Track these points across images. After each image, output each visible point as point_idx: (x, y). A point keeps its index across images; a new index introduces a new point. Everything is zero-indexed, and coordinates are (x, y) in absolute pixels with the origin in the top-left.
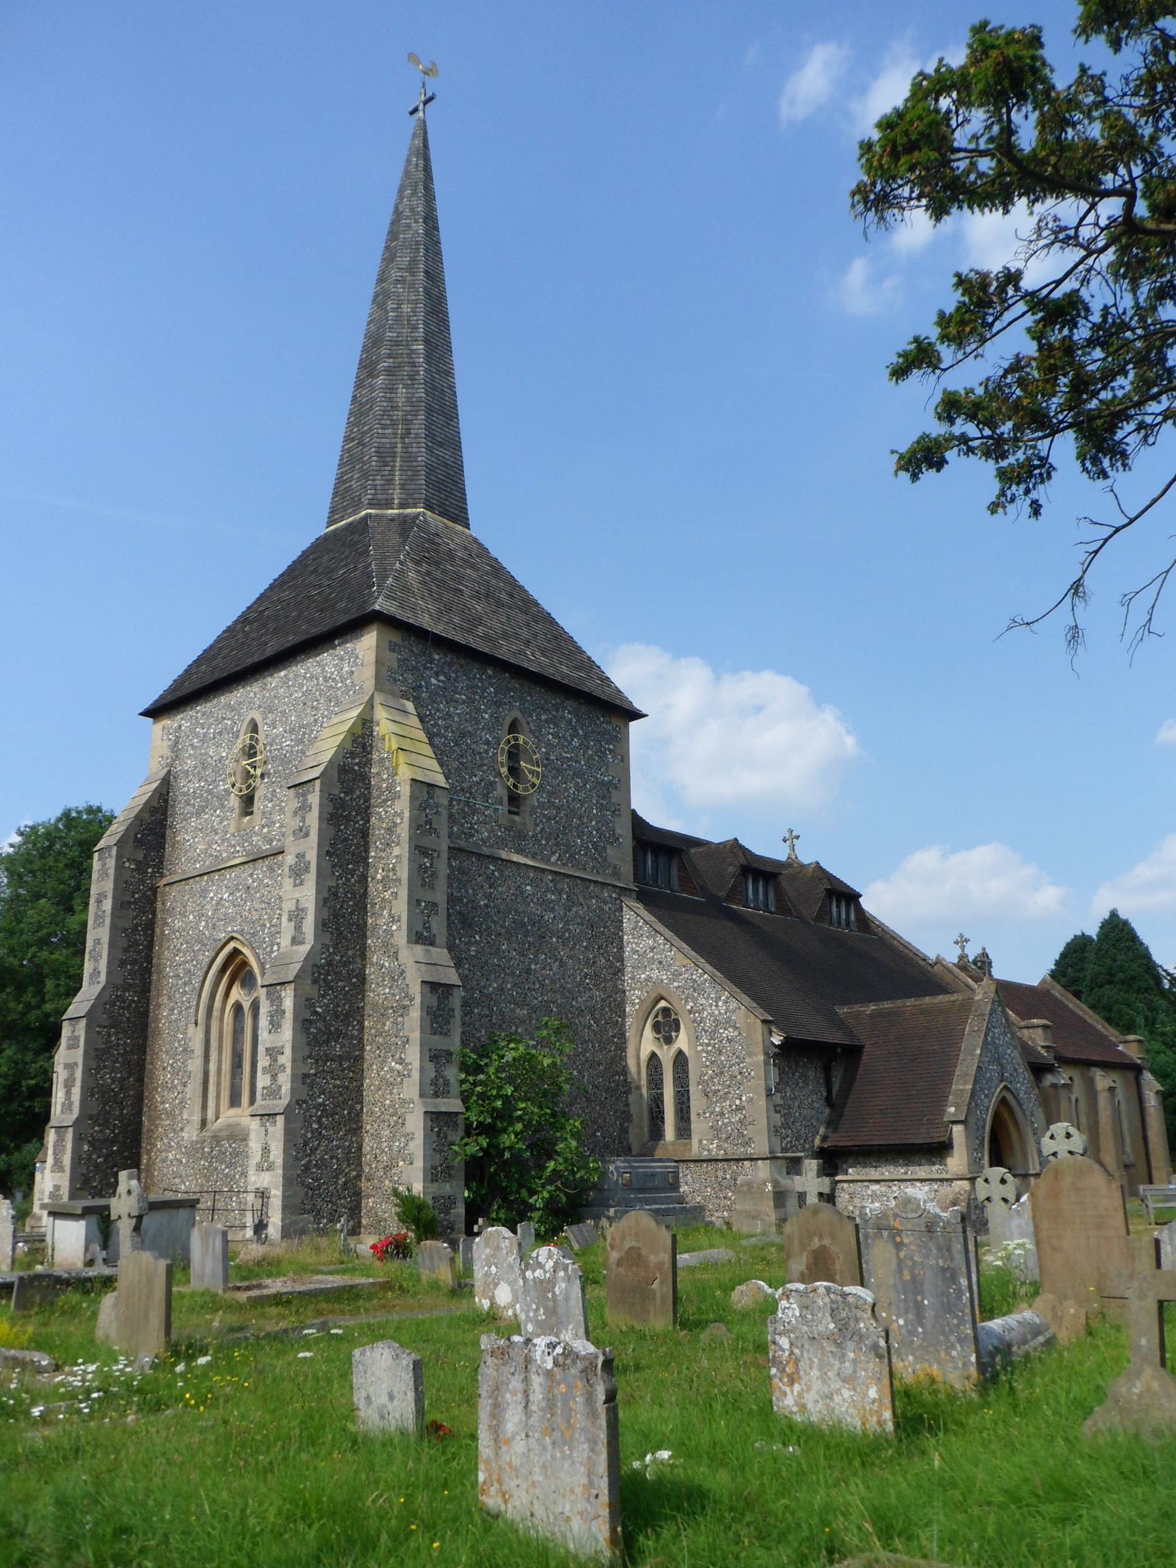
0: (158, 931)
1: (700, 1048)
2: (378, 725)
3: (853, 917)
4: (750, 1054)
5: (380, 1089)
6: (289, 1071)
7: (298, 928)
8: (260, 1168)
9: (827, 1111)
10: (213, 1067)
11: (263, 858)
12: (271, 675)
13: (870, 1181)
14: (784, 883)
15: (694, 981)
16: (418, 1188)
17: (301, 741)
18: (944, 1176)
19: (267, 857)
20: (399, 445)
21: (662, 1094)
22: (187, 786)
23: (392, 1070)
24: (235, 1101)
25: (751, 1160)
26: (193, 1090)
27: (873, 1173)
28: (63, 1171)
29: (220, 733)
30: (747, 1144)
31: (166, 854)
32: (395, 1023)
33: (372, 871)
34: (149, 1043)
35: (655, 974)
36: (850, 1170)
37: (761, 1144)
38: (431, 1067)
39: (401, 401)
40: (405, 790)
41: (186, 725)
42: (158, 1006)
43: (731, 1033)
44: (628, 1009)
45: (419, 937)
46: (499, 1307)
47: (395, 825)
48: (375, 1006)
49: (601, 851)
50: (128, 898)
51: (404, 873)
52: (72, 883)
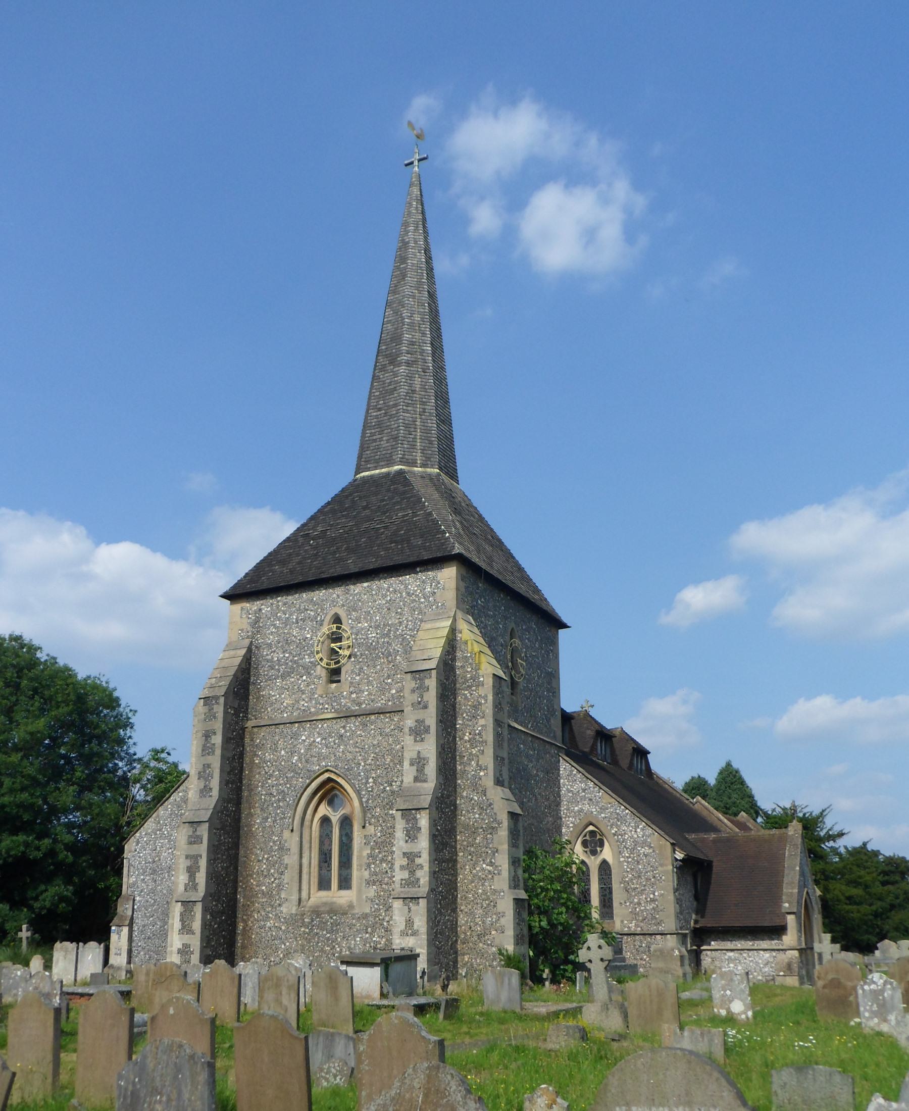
0: (247, 760)
1: (622, 859)
2: (461, 632)
3: (644, 768)
4: (661, 865)
5: (473, 882)
6: (426, 868)
7: (421, 770)
8: (404, 934)
9: (695, 903)
10: (305, 861)
11: (356, 716)
12: (354, 584)
13: (727, 950)
14: (616, 745)
15: (618, 814)
16: (510, 948)
17: (388, 635)
18: (781, 947)
19: (359, 716)
20: (419, 420)
21: (589, 889)
22: (272, 655)
23: (483, 870)
24: (324, 884)
25: (662, 934)
26: (289, 877)
27: (729, 945)
28: (193, 933)
29: (303, 620)
30: (659, 924)
31: (251, 703)
32: (485, 838)
33: (459, 734)
34: (243, 841)
35: (586, 808)
36: (713, 943)
37: (670, 923)
38: (512, 868)
39: (418, 388)
40: (489, 682)
41: (266, 609)
42: (251, 815)
43: (647, 850)
44: (564, 830)
45: (499, 782)
46: (733, 1014)
47: (480, 704)
48: (467, 827)
49: (548, 721)
50: (230, 735)
51: (489, 737)
52: (14, 699)
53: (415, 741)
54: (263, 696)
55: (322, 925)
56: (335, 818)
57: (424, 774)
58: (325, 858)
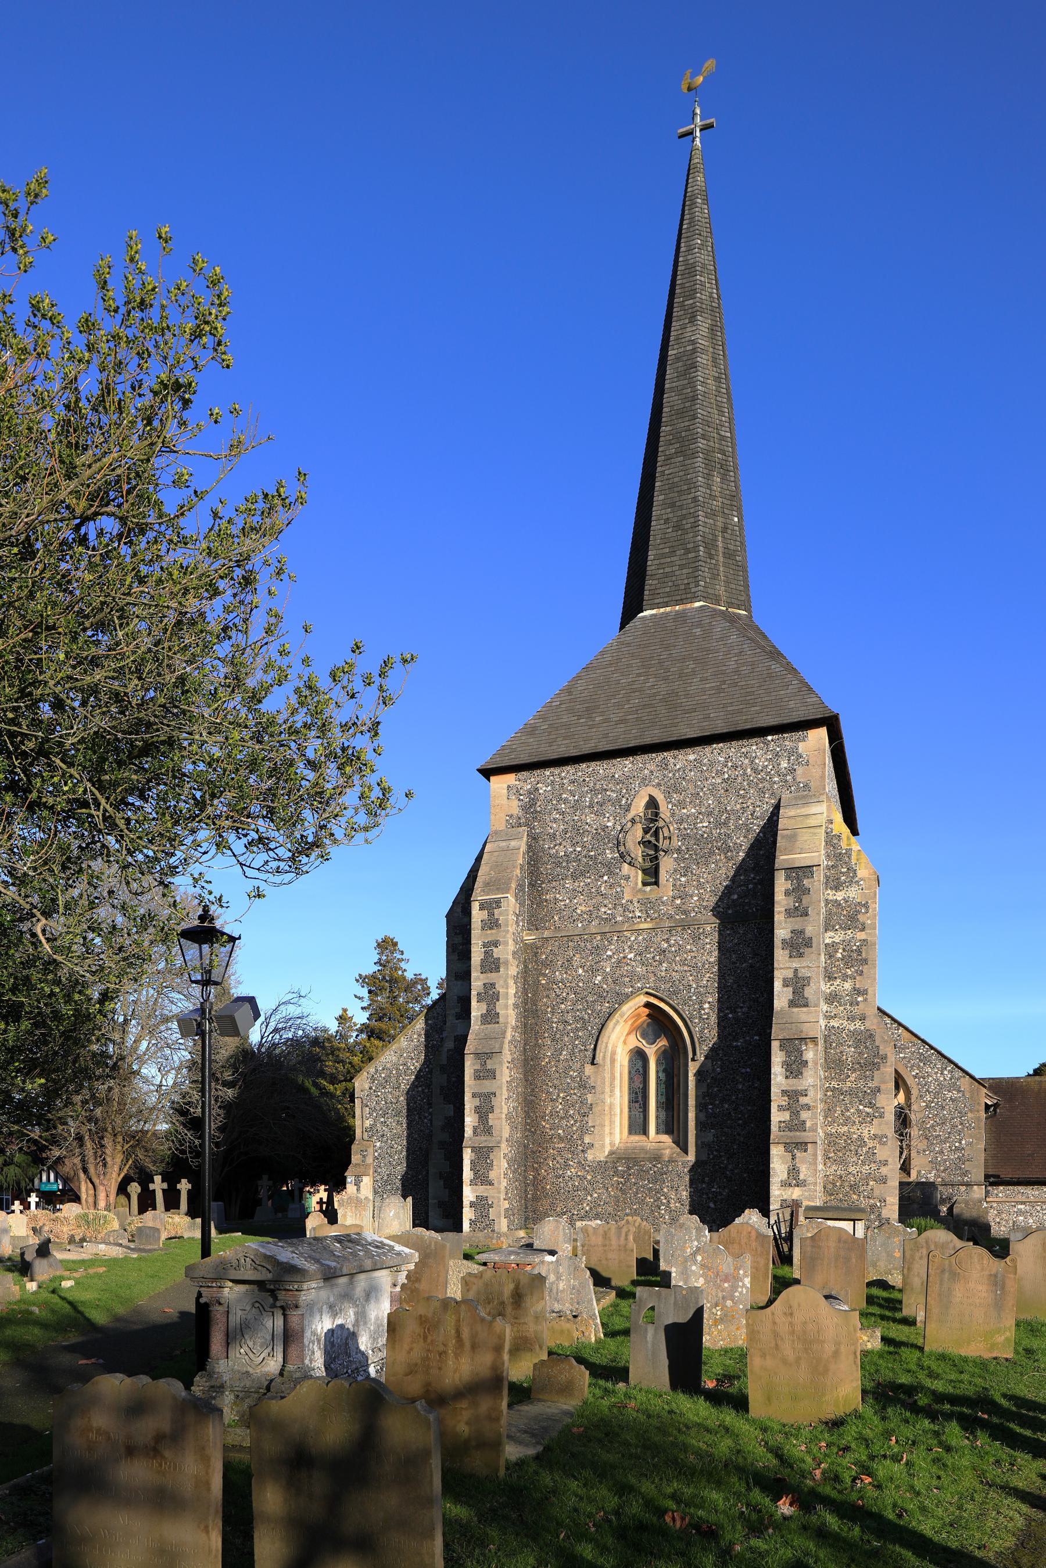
8: (786, 1184)
20: (720, 539)
23: (859, 1111)
24: (638, 1126)
47: (859, 912)
53: (790, 957)
54: (546, 901)
55: (642, 1173)
56: (652, 1052)
57: (804, 997)
58: (638, 1098)
